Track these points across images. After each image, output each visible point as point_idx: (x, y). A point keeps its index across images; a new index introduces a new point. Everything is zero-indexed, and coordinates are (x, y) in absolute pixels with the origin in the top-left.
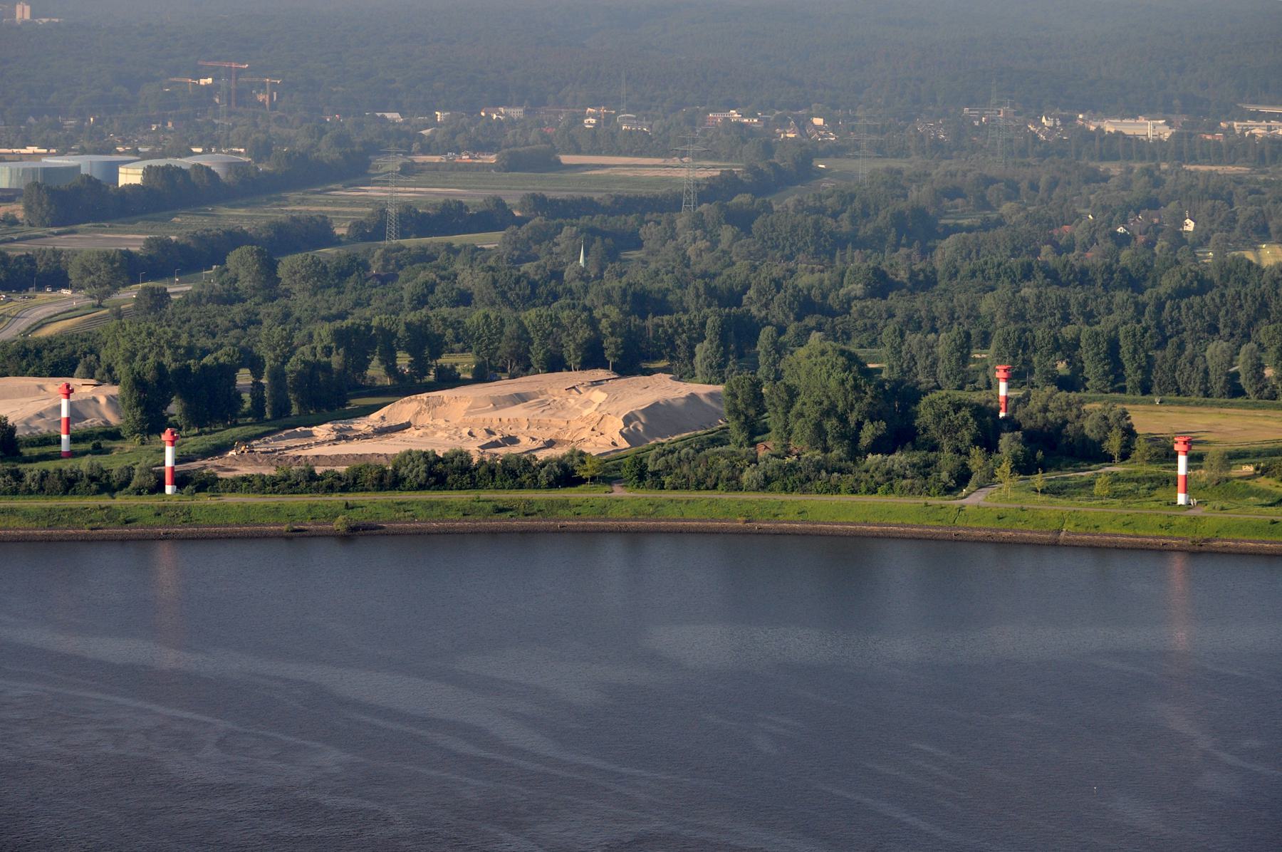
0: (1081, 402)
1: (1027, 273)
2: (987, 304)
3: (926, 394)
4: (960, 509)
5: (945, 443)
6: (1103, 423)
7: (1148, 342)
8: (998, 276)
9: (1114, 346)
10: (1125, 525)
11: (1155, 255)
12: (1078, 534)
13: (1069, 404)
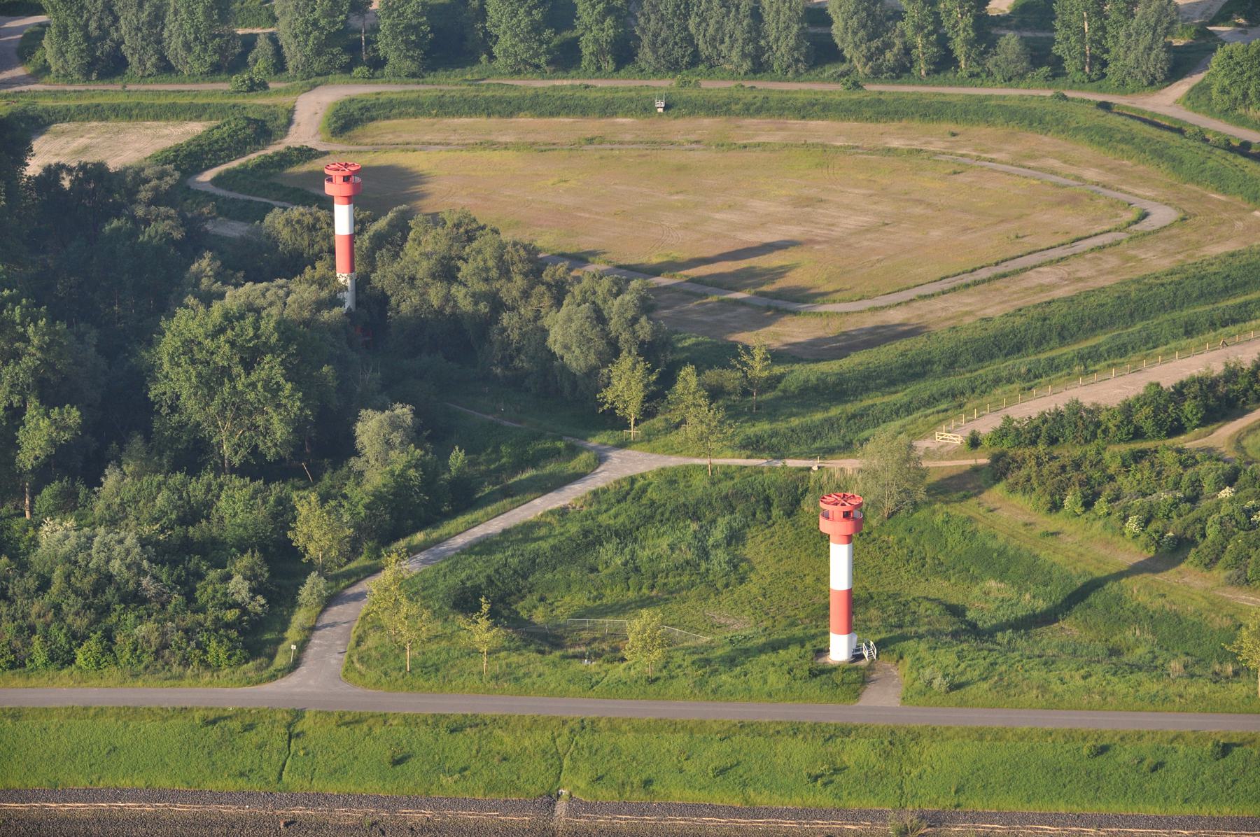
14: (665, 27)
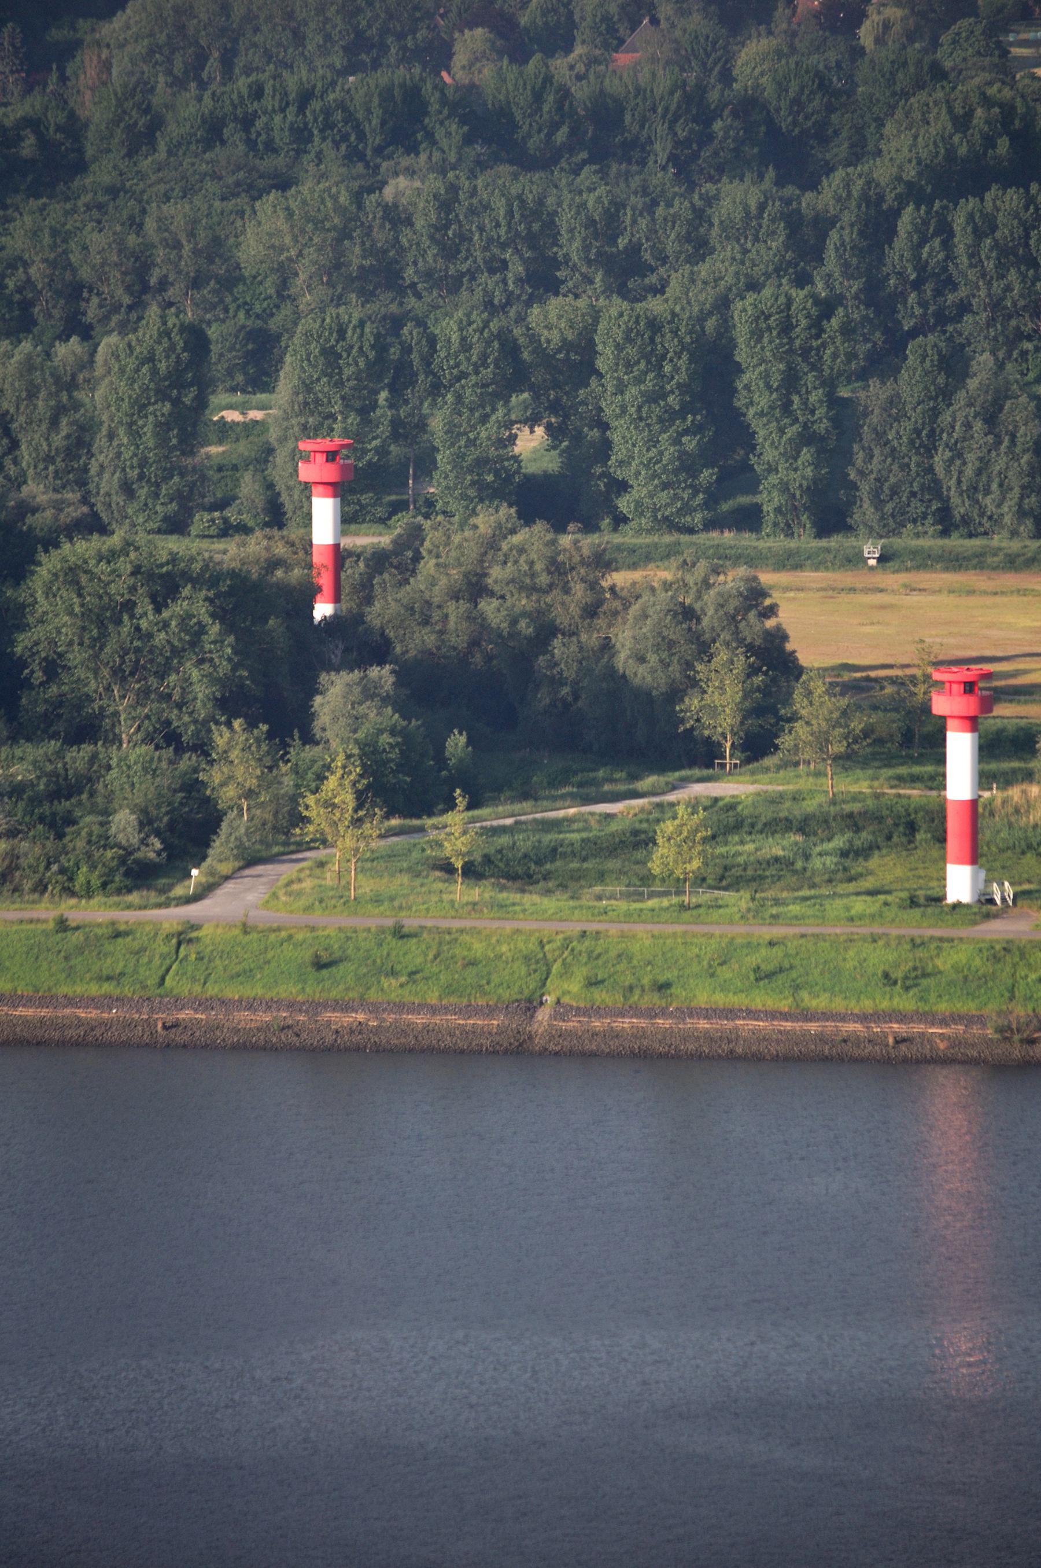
0: (602, 562)
1: (405, 125)
2: (262, 234)
3: (51, 543)
4: (184, 936)
5: (124, 709)
6: (675, 632)
7: (834, 352)
8: (301, 136)
9: (714, 367)
10: (763, 976)
11: (858, 52)
12: (596, 1011)
13: (557, 568)
14: (895, 467)
